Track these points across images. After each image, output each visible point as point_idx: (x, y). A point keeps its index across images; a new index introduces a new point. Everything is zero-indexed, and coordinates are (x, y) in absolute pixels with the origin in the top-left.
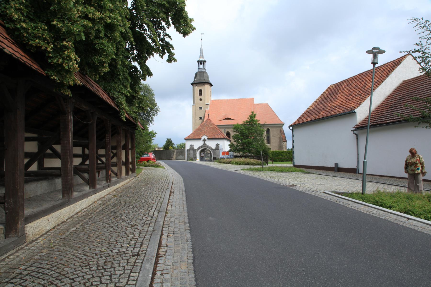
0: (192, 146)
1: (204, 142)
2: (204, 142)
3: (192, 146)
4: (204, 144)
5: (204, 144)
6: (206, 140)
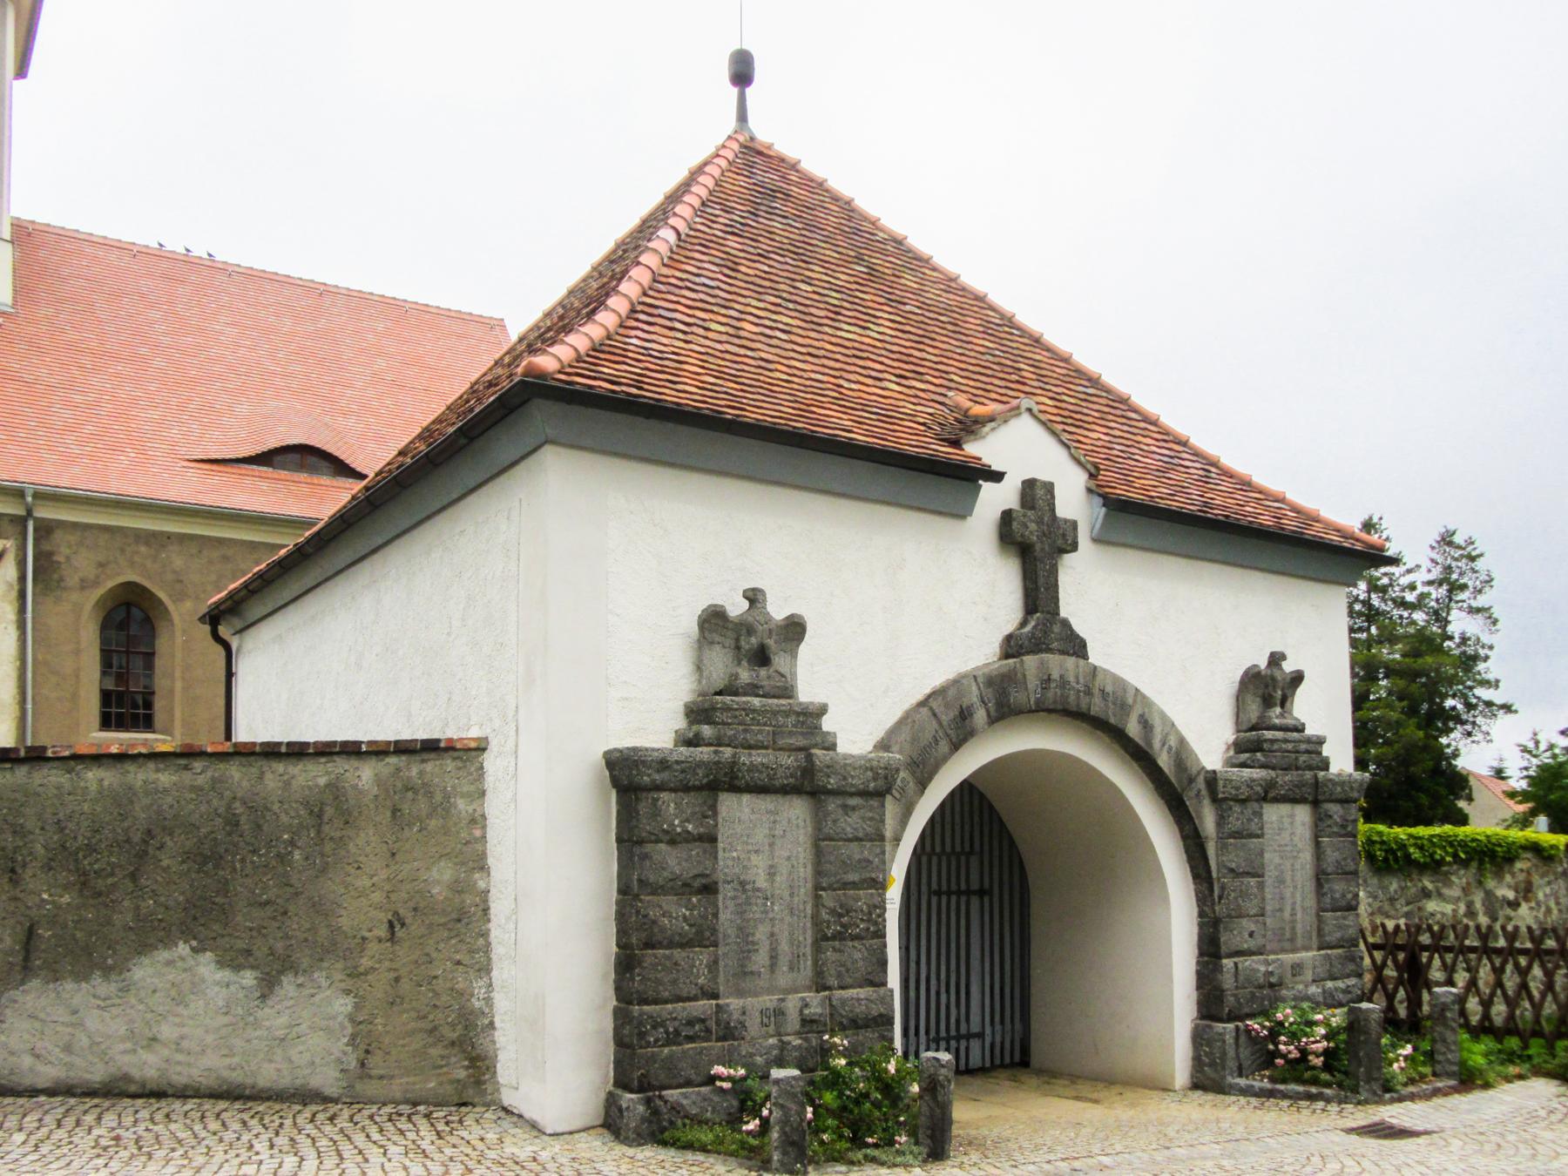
0: (748, 644)
1: (1039, 594)
2: (1039, 594)
3: (748, 644)
4: (1042, 626)
5: (1042, 626)
6: (1063, 540)
